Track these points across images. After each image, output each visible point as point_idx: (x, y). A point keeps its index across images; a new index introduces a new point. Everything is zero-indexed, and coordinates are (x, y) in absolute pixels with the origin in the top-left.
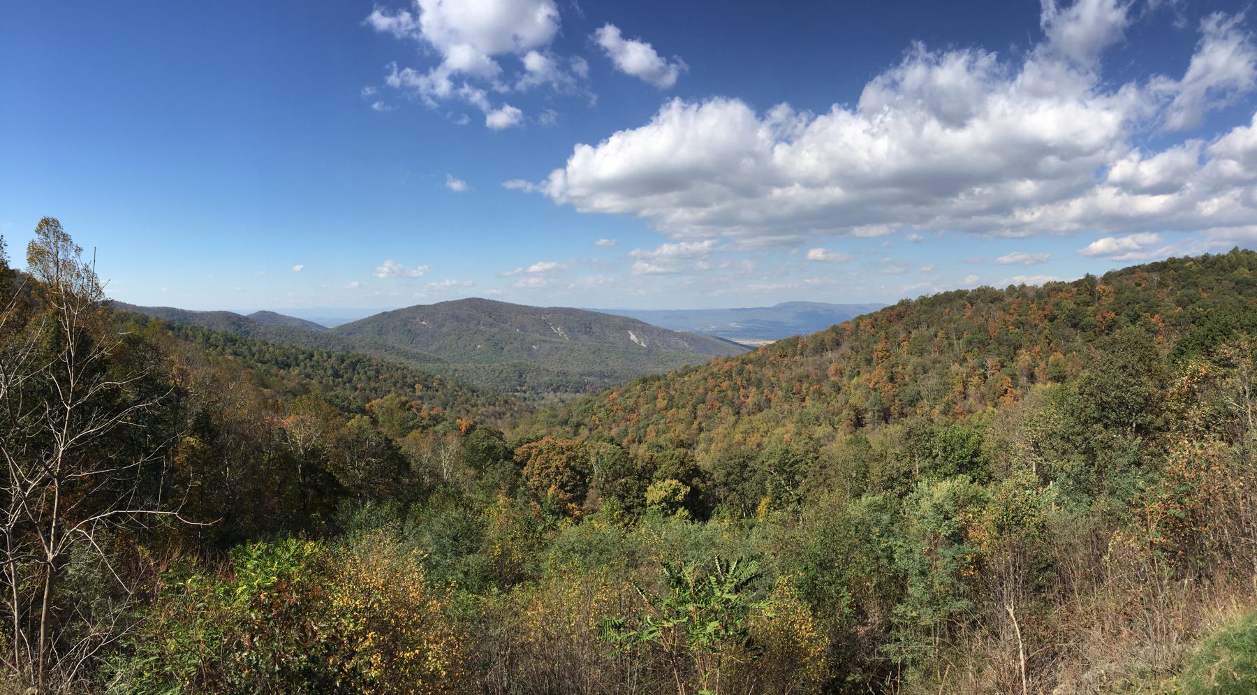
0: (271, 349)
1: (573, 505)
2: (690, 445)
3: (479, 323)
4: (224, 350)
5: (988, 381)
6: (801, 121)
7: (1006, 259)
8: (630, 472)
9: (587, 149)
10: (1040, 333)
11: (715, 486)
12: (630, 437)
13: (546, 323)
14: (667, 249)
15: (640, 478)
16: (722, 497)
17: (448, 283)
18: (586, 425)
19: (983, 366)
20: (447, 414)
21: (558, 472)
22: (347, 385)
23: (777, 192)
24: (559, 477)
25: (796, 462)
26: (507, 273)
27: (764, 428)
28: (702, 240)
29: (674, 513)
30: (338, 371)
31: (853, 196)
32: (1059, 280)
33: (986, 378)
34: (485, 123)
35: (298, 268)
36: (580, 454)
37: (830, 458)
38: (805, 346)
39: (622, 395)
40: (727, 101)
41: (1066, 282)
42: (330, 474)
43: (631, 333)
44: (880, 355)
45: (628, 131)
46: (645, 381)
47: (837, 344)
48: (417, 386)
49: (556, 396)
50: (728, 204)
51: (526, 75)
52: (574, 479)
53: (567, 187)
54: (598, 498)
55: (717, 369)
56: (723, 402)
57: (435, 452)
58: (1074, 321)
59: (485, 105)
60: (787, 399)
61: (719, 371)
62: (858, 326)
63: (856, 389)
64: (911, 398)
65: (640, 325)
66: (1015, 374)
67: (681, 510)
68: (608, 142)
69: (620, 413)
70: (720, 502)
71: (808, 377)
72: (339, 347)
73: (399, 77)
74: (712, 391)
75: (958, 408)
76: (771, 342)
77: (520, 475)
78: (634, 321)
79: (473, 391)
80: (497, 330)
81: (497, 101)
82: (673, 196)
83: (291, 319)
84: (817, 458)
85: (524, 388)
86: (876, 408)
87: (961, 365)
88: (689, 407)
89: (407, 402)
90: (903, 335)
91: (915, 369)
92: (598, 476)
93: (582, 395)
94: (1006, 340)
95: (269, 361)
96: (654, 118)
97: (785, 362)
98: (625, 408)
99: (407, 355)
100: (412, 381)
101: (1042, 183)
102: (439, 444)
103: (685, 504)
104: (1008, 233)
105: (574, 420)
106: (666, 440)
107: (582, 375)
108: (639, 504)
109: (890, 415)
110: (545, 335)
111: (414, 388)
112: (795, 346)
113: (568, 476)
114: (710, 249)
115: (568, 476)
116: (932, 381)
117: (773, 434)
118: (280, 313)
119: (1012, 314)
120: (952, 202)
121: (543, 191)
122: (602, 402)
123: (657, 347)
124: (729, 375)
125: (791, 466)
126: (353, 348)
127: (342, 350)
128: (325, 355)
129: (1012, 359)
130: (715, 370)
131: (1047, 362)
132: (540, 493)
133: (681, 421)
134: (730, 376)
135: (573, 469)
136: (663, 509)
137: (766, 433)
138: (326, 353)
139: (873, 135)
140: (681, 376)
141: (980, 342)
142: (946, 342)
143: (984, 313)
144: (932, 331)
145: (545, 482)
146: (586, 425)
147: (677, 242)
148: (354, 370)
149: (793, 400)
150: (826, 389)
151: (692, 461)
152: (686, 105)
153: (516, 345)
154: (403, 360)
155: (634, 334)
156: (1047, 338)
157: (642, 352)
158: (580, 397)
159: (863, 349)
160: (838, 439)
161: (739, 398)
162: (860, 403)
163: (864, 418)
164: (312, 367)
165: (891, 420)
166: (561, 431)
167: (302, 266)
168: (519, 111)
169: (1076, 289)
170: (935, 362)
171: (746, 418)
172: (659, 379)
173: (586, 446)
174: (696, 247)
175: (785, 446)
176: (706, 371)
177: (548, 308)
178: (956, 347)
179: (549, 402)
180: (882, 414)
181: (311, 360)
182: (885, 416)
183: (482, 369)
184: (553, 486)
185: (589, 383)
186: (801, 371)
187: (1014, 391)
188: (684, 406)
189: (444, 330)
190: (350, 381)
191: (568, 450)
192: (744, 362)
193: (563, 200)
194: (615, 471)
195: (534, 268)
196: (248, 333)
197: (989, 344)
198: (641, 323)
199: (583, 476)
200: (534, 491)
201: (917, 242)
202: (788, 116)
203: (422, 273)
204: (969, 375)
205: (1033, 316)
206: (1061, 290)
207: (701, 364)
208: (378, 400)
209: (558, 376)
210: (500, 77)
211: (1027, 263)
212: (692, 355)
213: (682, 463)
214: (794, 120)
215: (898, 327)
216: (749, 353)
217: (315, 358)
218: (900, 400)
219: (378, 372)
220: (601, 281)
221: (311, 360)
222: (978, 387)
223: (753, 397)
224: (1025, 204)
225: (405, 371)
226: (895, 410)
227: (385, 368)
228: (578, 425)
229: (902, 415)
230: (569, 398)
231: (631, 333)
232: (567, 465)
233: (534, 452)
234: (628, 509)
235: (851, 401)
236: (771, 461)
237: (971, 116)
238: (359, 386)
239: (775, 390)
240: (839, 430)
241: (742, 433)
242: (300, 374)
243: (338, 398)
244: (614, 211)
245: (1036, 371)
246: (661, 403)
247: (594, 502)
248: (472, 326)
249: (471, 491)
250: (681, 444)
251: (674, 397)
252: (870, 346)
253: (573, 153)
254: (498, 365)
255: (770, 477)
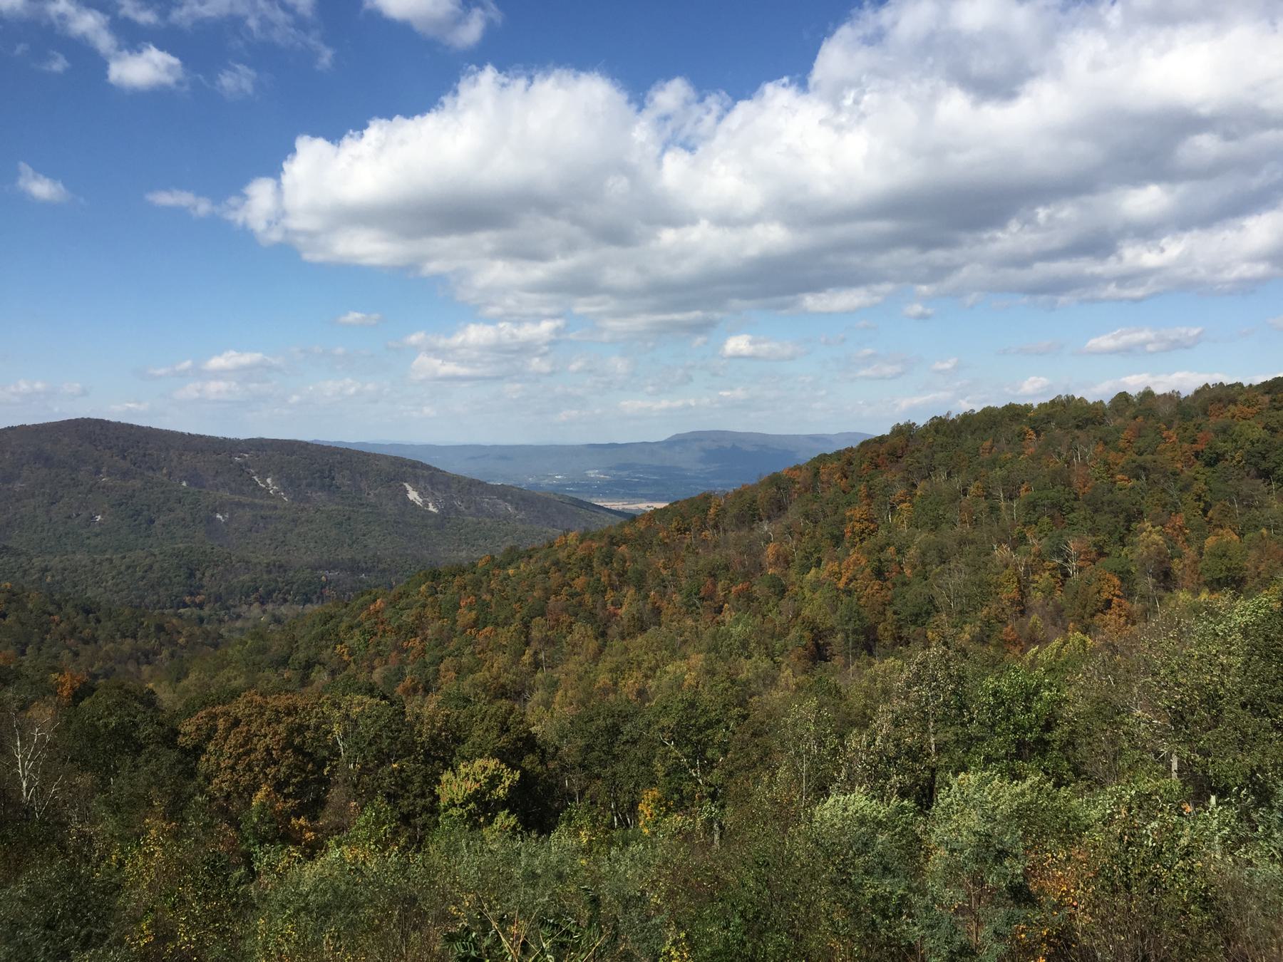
1: (302, 821)
2: (519, 694)
5: (1069, 582)
7: (1105, 342)
8: (409, 749)
9: (320, 145)
10: (1185, 488)
11: (563, 769)
12: (408, 681)
13: (242, 468)
14: (476, 334)
15: (429, 759)
16: (576, 790)
18: (323, 664)
19: (1059, 553)
20: (27, 664)
21: (270, 760)
23: (668, 236)
24: (271, 771)
25: (709, 725)
27: (649, 660)
28: (538, 318)
29: (490, 822)
31: (806, 239)
32: (1228, 381)
33: (1066, 575)
34: (107, 76)
38: (722, 511)
39: (392, 604)
40: (576, 77)
41: (1246, 384)
43: (409, 488)
44: (858, 527)
45: (398, 119)
46: (435, 576)
47: (779, 507)
49: (264, 612)
53: (281, 214)
54: (348, 802)
55: (565, 554)
58: (1264, 465)
59: (105, 42)
60: (690, 609)
61: (569, 557)
62: (816, 474)
63: (814, 591)
64: (916, 610)
65: (426, 473)
66: (1129, 571)
67: (502, 815)
68: (362, 135)
70: (572, 800)
71: (727, 568)
74: (557, 594)
75: (1009, 631)
76: (660, 505)
77: (192, 774)
78: (415, 465)
79: (87, 612)
80: (138, 483)
82: (485, 239)
84: (745, 717)
85: (198, 599)
86: (850, 627)
87: (1014, 549)
88: (516, 624)
90: (900, 491)
91: (924, 554)
93: (316, 607)
94: (1110, 503)
96: (447, 100)
97: (687, 541)
101: (1182, 189)
104: (1112, 289)
105: (301, 655)
106: (474, 685)
108: (424, 808)
109: (876, 640)
110: (242, 493)
112: (705, 511)
113: (288, 767)
114: (553, 337)
115: (288, 767)
116: (955, 579)
117: (666, 672)
119: (1124, 451)
120: (993, 240)
121: (231, 216)
122: (355, 617)
123: (458, 512)
124: (586, 565)
125: (700, 731)
129: (1121, 539)
130: (562, 555)
131: (1201, 548)
132: (236, 805)
133: (501, 648)
134: (590, 566)
135: (299, 750)
136: (470, 813)
137: (653, 670)
139: (839, 129)
140: (502, 566)
141: (1053, 505)
142: (984, 505)
143: (1063, 450)
144: (957, 482)
145: (245, 780)
146: (323, 664)
147: (492, 321)
149: (701, 611)
150: (759, 590)
151: (522, 722)
152: (506, 80)
155: (415, 489)
156: (1199, 498)
157: (430, 522)
158: (313, 608)
159: (825, 516)
160: (782, 682)
161: (604, 606)
162: (821, 616)
163: (829, 644)
165: (878, 649)
166: (275, 679)
168: (174, 61)
169: (1267, 398)
170: (962, 542)
171: (617, 644)
174: (528, 331)
175: (688, 695)
176: (546, 557)
177: (246, 441)
178: (1004, 514)
179: (250, 624)
180: (862, 638)
182: (868, 643)
183: (106, 565)
185: (329, 582)
186: (716, 557)
187: (1127, 604)
188: (506, 623)
191: (289, 714)
192: (614, 542)
193: (275, 236)
194: (380, 751)
195: (217, 362)
197: (1073, 510)
198: (428, 468)
201: (922, 317)
202: (687, 103)
204: (1031, 570)
205: (1168, 455)
206: (1233, 401)
209: (270, 572)
211: (1150, 348)
213: (504, 730)
215: (892, 476)
218: (895, 613)
220: (352, 390)
222: (1049, 592)
224: (1147, 232)
226: (885, 631)
228: (309, 665)
229: (900, 640)
231: (409, 488)
232: (288, 744)
233: (221, 724)
234: (406, 819)
235: (806, 612)
236: (664, 722)
237: (1032, 74)
239: (669, 591)
241: (611, 671)
244: (376, 261)
245: (1176, 565)
246: (466, 616)
247: (341, 810)
250: (502, 692)
251: (488, 605)
252: (841, 510)
253: (293, 150)
254: (141, 553)
255: (661, 750)
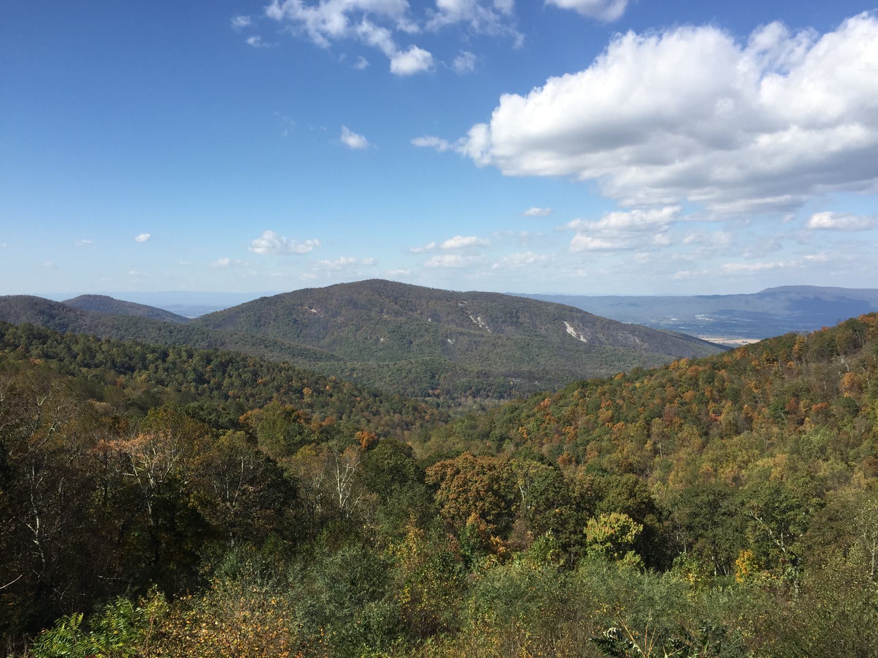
0: (105, 347)
2: (642, 471)
3: (382, 312)
4: (27, 350)
6: (799, 44)
8: (567, 501)
11: (675, 528)
13: (463, 310)
14: (616, 219)
17: (343, 260)
18: (511, 439)
21: (479, 497)
22: (215, 392)
23: (764, 140)
25: (791, 508)
26: (417, 250)
27: (742, 456)
28: (661, 206)
29: (622, 557)
30: (202, 375)
34: (389, 69)
35: (143, 237)
36: (505, 475)
37: (844, 506)
42: (194, 509)
43: (567, 325)
47: (855, 346)
48: (305, 390)
49: (475, 402)
50: (696, 161)
51: (438, 14)
52: (498, 506)
53: (490, 146)
54: (526, 530)
55: (678, 374)
56: (685, 418)
57: (329, 474)
59: (388, 47)
60: (776, 419)
61: (680, 376)
65: (579, 315)
67: (630, 555)
69: (553, 425)
71: (808, 390)
72: (203, 344)
73: (281, 8)
74: (671, 402)
77: (431, 500)
78: (572, 309)
80: (403, 319)
81: (403, 42)
82: (624, 152)
83: (133, 306)
84: (822, 506)
88: (641, 422)
89: (293, 411)
92: (526, 505)
95: (101, 363)
97: (775, 369)
98: (559, 418)
99: (295, 353)
100: (299, 384)
102: (334, 464)
103: (638, 546)
105: (497, 432)
106: (610, 462)
107: (506, 376)
110: (462, 326)
111: (302, 394)
112: (791, 347)
113: (490, 503)
115: (490, 503)
118: (116, 297)
122: (531, 410)
123: (600, 342)
124: (694, 382)
125: (784, 512)
126: (223, 344)
127: (208, 347)
128: (184, 354)
130: (675, 375)
135: (496, 493)
137: (746, 463)
138: (186, 351)
140: (631, 381)
145: (464, 508)
146: (511, 439)
148: (224, 372)
149: (786, 421)
151: (645, 491)
153: (427, 338)
154: (287, 358)
155: (572, 326)
158: (505, 403)
161: (707, 414)
164: (166, 370)
166: (481, 446)
167: (148, 235)
168: (428, 54)
172: (603, 383)
173: (511, 465)
174: (654, 216)
176: (663, 376)
179: (466, 410)
181: (164, 361)
183: (385, 369)
184: (473, 514)
185: (515, 386)
186: (799, 381)
188: (634, 420)
189: (339, 320)
190: (219, 387)
191: (490, 470)
192: (715, 367)
193: (486, 161)
194: (547, 499)
195: (450, 243)
196: (64, 326)
198: (581, 311)
199: (509, 503)
200: (449, 520)
202: (781, 39)
203: (310, 249)
207: (656, 366)
208: (256, 411)
210: (406, 15)
212: (645, 354)
214: (790, 44)
216: (722, 355)
217: (171, 358)
219: (255, 374)
220: (532, 260)
221: (164, 361)
223: (726, 414)
225: (290, 372)
227: (265, 370)
228: (502, 439)
230: (491, 404)
231: (567, 325)
232: (489, 488)
233: (449, 471)
234: (565, 547)
236: (754, 502)
238: (231, 393)
239: (760, 405)
240: (856, 469)
241: (712, 460)
242: (148, 380)
243: (202, 409)
244: (549, 173)
246: (605, 414)
248: (373, 314)
249: (373, 521)
253: (498, 104)
254: (405, 362)
